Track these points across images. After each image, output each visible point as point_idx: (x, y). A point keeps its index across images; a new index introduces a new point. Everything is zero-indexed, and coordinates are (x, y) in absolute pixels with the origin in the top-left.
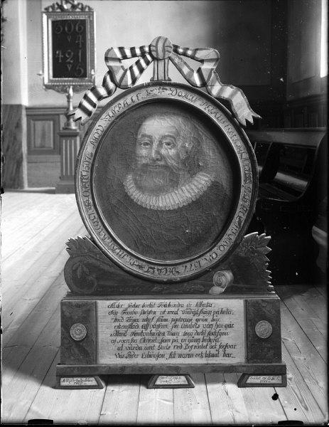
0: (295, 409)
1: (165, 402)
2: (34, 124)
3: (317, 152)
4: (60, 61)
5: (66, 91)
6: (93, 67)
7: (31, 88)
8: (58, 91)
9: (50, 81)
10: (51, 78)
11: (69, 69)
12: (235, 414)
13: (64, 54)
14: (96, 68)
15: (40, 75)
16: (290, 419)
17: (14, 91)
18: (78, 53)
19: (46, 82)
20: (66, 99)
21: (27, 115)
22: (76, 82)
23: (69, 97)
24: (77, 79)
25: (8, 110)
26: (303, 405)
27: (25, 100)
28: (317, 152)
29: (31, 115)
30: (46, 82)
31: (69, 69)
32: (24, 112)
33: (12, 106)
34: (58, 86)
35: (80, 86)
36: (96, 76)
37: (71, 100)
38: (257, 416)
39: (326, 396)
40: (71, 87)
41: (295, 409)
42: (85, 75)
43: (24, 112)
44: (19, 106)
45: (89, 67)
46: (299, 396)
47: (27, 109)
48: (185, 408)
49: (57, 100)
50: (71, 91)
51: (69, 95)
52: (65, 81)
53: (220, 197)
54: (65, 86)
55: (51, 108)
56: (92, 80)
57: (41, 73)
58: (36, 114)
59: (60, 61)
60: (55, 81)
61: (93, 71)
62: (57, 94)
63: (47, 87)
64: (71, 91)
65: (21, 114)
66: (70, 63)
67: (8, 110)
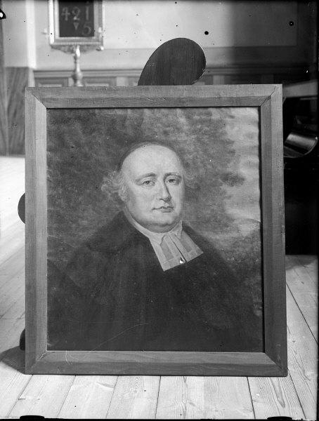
0: (207, 33)
1: (104, 387)
2: (210, 68)
3: (298, 91)
4: (66, 19)
5: (73, 52)
6: (101, 25)
7: (39, 50)
8: (65, 52)
9: (56, 40)
10: (57, 37)
11: (76, 27)
12: (188, 405)
13: (70, 11)
14: (104, 26)
15: (44, 34)
16: (258, 418)
17: (22, 52)
18: (85, 10)
19: (52, 41)
20: (73, 60)
21: (36, 79)
22: (83, 41)
23: (75, 58)
24: (84, 38)
25: (15, 73)
26: (280, 399)
27: (33, 63)
28: (298, 91)
29: (40, 79)
30: (52, 41)
31: (76, 27)
32: (31, 76)
33: (19, 69)
34: (64, 46)
35: (88, 45)
36: (104, 35)
37: (78, 61)
38: (216, 411)
39: (316, 400)
40: (78, 47)
41: (207, 33)
42: (92, 34)
43: (31, 76)
44: (26, 69)
45: (96, 25)
46: (277, 388)
47: (35, 72)
48: (127, 395)
49: (62, 62)
50: (78, 52)
51: (76, 55)
52: (78, 41)
53: (247, 249)
54: (71, 46)
55: (130, 70)
56: (100, 40)
57: (46, 31)
58: (44, 77)
59: (66, 19)
60: (63, 41)
61: (100, 29)
62: (65, 54)
63: (53, 47)
64: (78, 52)
65: (28, 77)
66: (76, 21)
67: (15, 73)
